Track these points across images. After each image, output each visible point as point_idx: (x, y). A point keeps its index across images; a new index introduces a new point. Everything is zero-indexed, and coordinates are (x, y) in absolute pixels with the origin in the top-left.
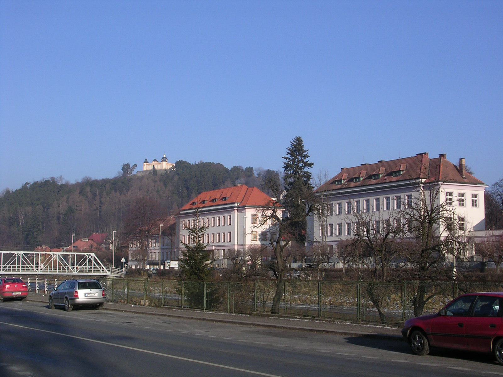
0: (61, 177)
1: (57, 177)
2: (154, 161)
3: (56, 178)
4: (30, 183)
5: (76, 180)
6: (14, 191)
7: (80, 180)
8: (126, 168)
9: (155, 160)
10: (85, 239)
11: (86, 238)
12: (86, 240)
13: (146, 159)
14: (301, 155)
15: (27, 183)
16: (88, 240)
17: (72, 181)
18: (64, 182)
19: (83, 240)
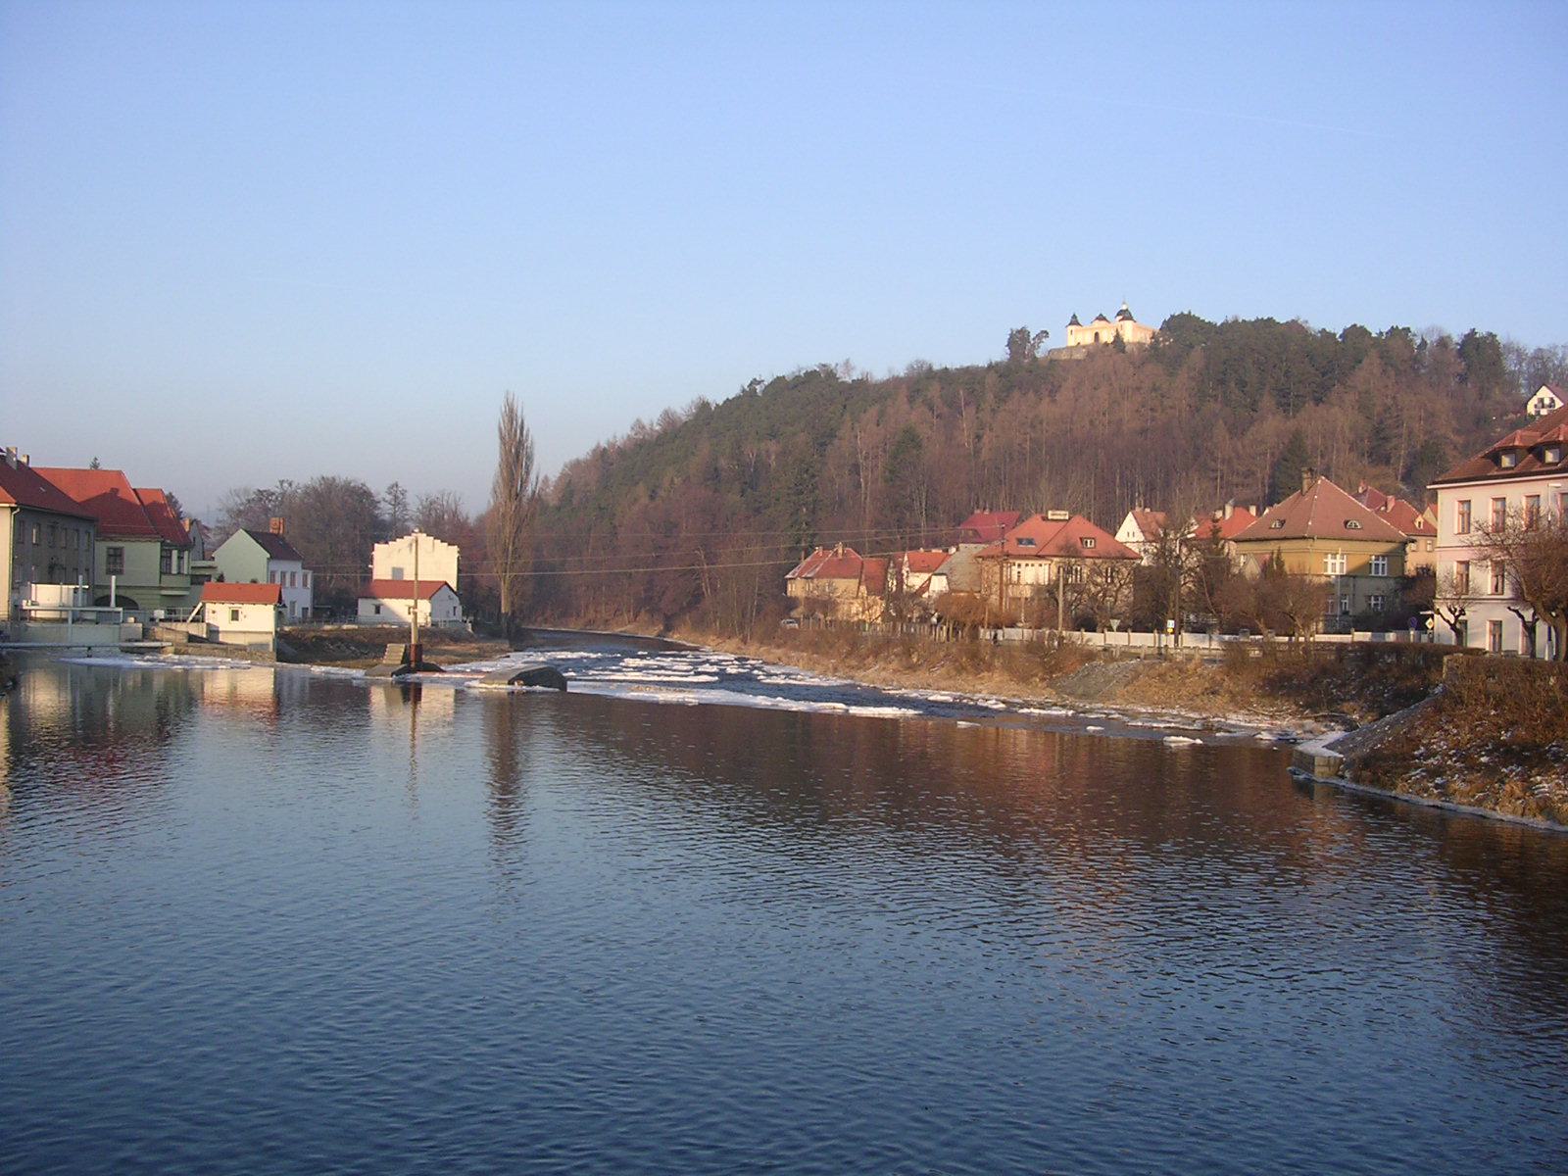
0: (847, 363)
1: (837, 365)
3: (833, 365)
5: (890, 371)
8: (1019, 340)
9: (1101, 318)
10: (1058, 512)
13: (1074, 316)
14: (1157, 341)
15: (755, 382)
16: (1067, 518)
17: (880, 374)
19: (1050, 517)
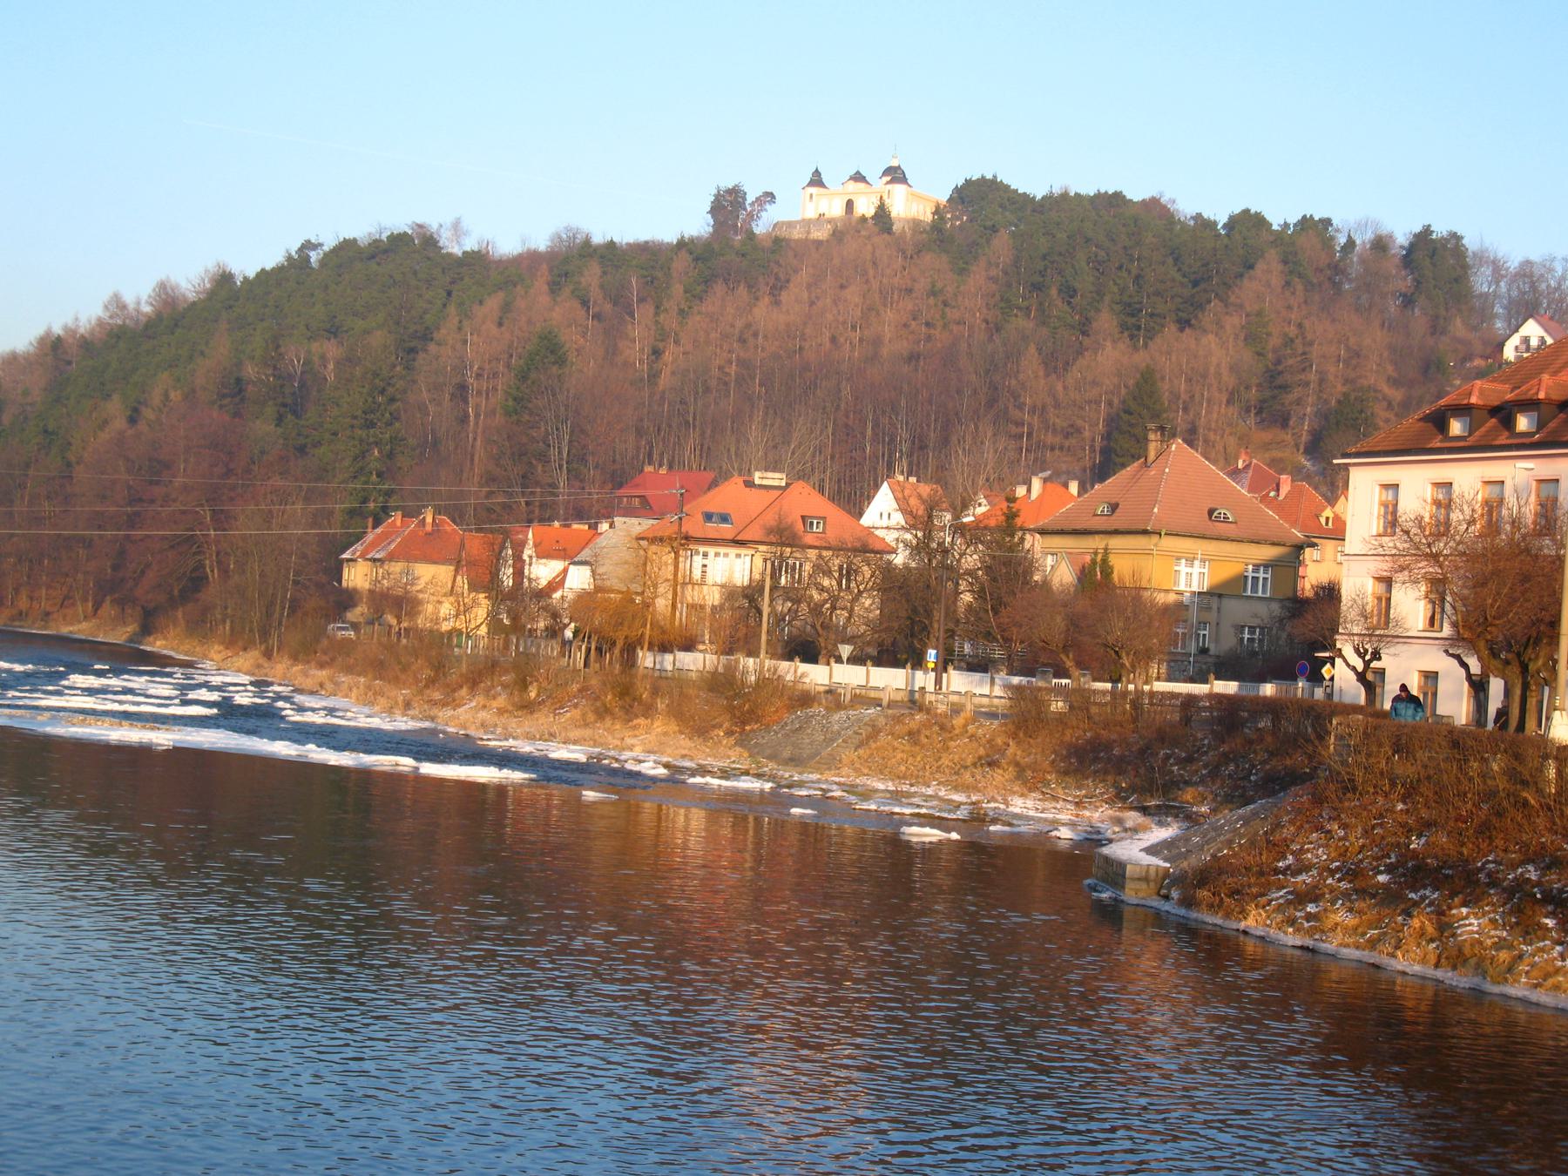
2: (851, 182)
4: (321, 245)
6: (251, 274)
7: (541, 243)
8: (728, 205)
10: (770, 475)
11: (774, 470)
12: (776, 483)
13: (817, 173)
15: (308, 246)
16: (783, 484)
17: (507, 245)
18: (470, 244)
